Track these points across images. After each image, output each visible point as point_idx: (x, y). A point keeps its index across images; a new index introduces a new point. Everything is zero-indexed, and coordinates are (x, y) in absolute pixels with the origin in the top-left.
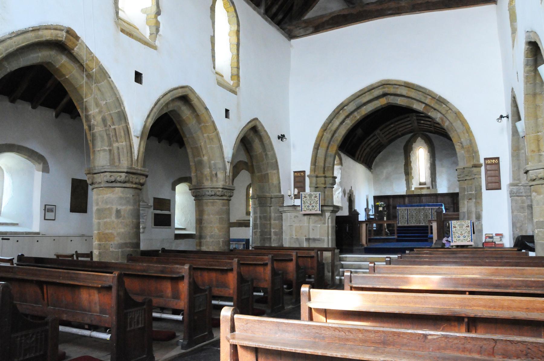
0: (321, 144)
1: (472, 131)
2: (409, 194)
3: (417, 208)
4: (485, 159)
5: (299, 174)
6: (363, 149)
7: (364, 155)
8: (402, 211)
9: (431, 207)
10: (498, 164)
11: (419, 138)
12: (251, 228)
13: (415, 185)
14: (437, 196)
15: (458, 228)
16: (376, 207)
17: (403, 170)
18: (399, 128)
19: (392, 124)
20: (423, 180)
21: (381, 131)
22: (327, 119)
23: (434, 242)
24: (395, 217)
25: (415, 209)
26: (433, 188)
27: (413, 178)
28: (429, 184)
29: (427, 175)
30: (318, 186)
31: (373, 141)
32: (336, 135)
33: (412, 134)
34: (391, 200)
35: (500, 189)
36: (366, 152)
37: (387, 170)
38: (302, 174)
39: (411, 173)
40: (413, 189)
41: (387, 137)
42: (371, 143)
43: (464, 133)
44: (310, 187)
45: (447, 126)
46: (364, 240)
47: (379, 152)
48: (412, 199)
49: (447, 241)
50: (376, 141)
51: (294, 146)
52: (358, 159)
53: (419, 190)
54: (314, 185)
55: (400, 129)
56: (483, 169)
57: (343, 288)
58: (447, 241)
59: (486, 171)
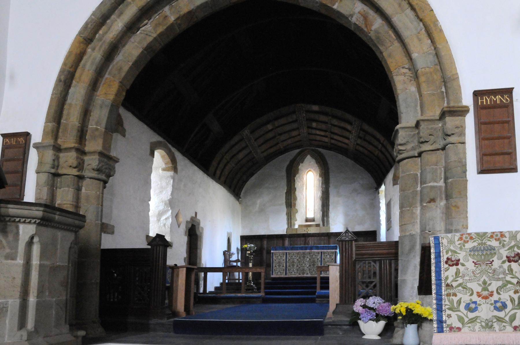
0: (77, 75)
1: (443, 28)
2: (290, 233)
3: (301, 251)
4: (477, 94)
5: (13, 141)
6: (224, 161)
7: (226, 172)
8: (278, 256)
9: (320, 251)
10: (509, 107)
11: (309, 157)
12: (434, 295)
13: (299, 222)
14: (330, 236)
15: (470, 265)
16: (243, 251)
17: (284, 201)
18: (280, 134)
19: (268, 123)
20: (310, 215)
21: (252, 132)
22: (94, 14)
23: (332, 307)
24: (269, 266)
25: (298, 253)
26: (324, 225)
27: (297, 212)
28: (319, 221)
29: (316, 208)
30: (60, 171)
31: (240, 151)
32: (119, 58)
33: (297, 151)
34: (265, 242)
35: (514, 170)
36: (228, 168)
37: (262, 199)
38: (21, 140)
39: (295, 204)
40: (296, 227)
41: (264, 147)
42: (238, 153)
43: (420, 40)
44: (38, 172)
45: (377, 32)
46: (180, 305)
47: (252, 175)
48: (295, 240)
49: (364, 306)
50: (245, 152)
51: (12, 78)
52: (220, 178)
53: (305, 229)
54: (47, 167)
55: (283, 137)
56: (470, 120)
57: (328, 278)
58: (364, 306)
59: (480, 124)
